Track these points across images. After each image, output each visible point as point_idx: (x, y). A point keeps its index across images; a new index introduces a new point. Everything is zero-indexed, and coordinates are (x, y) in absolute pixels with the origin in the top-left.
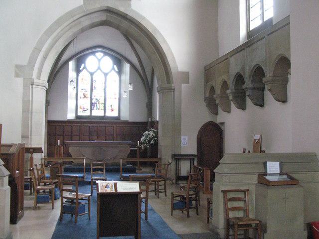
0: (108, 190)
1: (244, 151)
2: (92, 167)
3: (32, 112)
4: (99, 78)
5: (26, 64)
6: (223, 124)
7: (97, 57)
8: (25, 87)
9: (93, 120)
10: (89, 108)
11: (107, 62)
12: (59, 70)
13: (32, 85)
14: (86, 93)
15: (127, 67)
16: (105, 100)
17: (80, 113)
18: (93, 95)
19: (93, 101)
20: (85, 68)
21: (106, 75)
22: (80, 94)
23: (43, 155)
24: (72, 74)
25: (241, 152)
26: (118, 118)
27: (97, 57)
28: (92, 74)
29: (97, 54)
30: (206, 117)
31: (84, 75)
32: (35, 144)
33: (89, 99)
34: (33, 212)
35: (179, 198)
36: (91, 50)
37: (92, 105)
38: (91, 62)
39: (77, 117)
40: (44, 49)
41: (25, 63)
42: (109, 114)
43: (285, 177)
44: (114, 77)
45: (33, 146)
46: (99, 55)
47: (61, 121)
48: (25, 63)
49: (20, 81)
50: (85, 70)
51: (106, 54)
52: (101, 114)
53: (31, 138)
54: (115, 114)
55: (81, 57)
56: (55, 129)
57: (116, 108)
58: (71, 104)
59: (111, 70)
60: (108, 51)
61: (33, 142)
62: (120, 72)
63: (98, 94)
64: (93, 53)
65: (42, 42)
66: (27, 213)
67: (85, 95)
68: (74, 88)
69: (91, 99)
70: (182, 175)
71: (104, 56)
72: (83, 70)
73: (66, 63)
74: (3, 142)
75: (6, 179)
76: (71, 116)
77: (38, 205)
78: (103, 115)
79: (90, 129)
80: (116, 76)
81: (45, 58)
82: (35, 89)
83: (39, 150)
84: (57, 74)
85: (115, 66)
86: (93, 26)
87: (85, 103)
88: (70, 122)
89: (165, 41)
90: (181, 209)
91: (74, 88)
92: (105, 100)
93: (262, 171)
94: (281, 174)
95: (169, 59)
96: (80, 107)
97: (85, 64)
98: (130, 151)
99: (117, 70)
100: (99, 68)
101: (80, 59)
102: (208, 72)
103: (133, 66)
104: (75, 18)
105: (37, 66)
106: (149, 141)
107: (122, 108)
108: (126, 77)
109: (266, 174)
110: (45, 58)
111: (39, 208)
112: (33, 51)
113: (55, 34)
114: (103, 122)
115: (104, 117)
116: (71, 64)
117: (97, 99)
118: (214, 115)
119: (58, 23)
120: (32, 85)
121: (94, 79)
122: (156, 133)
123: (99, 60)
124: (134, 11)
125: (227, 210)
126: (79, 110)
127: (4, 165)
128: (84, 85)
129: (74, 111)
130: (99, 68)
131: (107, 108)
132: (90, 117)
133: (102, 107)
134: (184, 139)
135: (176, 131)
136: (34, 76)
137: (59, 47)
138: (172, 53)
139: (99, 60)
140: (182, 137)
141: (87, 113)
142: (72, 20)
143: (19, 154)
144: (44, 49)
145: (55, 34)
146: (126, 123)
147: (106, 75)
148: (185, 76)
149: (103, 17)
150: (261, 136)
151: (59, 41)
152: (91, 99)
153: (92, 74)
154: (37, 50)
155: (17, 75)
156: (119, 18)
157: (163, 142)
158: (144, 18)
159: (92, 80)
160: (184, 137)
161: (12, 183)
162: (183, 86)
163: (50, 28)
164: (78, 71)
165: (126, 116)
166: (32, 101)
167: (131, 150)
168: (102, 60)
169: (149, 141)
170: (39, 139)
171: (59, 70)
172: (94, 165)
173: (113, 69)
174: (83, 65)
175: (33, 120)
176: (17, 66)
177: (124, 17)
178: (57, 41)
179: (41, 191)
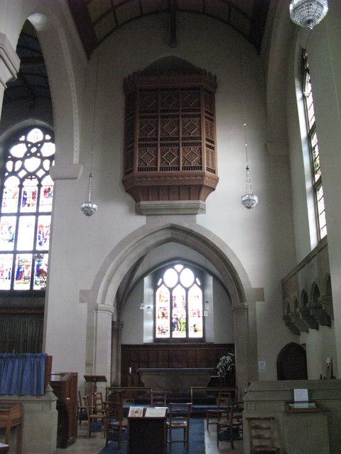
0: (137, 415)
1: (321, 378)
2: (152, 397)
3: (96, 339)
4: (179, 293)
5: (89, 288)
6: (305, 345)
7: (176, 270)
8: (90, 312)
9: (173, 344)
10: (169, 329)
11: (188, 276)
12: (133, 288)
13: (96, 310)
14: (165, 312)
15: (210, 280)
16: (187, 319)
17: (159, 336)
18: (173, 314)
19: (174, 320)
20: (163, 283)
21: (187, 290)
22: (159, 313)
23: (108, 384)
24: (148, 291)
25: (318, 378)
27: (176, 270)
28: (171, 290)
29: (176, 267)
30: (287, 338)
31: (162, 291)
33: (169, 318)
34: (87, 441)
35: (225, 429)
36: (169, 263)
37: (173, 326)
38: (170, 276)
39: (156, 340)
40: (108, 273)
41: (89, 287)
42: (192, 335)
43: (313, 404)
44: (196, 292)
45: (97, 375)
46: (179, 267)
47: (330, 287)
48: (89, 287)
50: (163, 285)
51: (185, 266)
52: (182, 335)
53: (95, 366)
54: (199, 335)
55: (157, 271)
57: (200, 327)
58: (148, 324)
59: (193, 285)
60: (188, 263)
61: (97, 370)
62: (203, 287)
63: (179, 312)
64: (172, 266)
65: (105, 266)
66: (79, 441)
67: (163, 315)
68: (11, 241)
69: (171, 319)
71: (184, 268)
72: (160, 285)
73: (141, 279)
75: (54, 404)
76: (148, 339)
77: (92, 434)
78: (185, 336)
79: (170, 353)
80: (199, 292)
81: (109, 281)
83: (103, 379)
85: (197, 279)
86: (168, 241)
87: (163, 323)
88: (146, 346)
89: (234, 255)
90: (228, 440)
91: (11, 241)
92: (187, 319)
93: (288, 398)
94: (310, 401)
95: (241, 276)
96: (159, 328)
97: (162, 278)
98: (210, 379)
99: (199, 283)
100: (179, 282)
101: (157, 273)
102: (284, 286)
103: (216, 278)
104: (138, 239)
105: (101, 291)
106: (226, 367)
107: (206, 328)
108: (210, 292)
109: (293, 402)
110: (109, 281)
111: (94, 437)
112: (97, 276)
113: (119, 256)
114: (187, 343)
115: (187, 340)
116: (147, 280)
117: (177, 319)
118: (295, 336)
119: (121, 245)
120: (96, 310)
121: (173, 295)
122: (233, 358)
123: (179, 274)
124: (198, 226)
125: (252, 437)
126: (157, 331)
127: (53, 392)
129: (152, 333)
130: (179, 282)
131: (190, 329)
132: (171, 339)
133: (183, 327)
134: (262, 364)
135: (253, 355)
136: (99, 301)
137: (133, 258)
138: (243, 269)
139: (179, 274)
140: (259, 362)
141: (167, 336)
142: (135, 241)
144: (108, 273)
145: (119, 256)
146: (211, 345)
147: (187, 290)
148: (260, 293)
149: (168, 235)
150: (331, 360)
151: (123, 263)
152: (171, 319)
153: (171, 290)
154: (101, 274)
155: (82, 301)
156: (185, 235)
157: (240, 369)
158: (210, 233)
159: (171, 297)
160: (262, 362)
161: (61, 408)
162: (258, 303)
163: (114, 250)
164: (155, 287)
165: (211, 338)
166: (96, 327)
167: (212, 378)
168: (182, 273)
169: (226, 367)
171: (133, 288)
172: (155, 395)
173: (195, 282)
174: (161, 280)
175: (98, 347)
176: (82, 292)
177: (190, 233)
178: (121, 263)
179: (98, 419)
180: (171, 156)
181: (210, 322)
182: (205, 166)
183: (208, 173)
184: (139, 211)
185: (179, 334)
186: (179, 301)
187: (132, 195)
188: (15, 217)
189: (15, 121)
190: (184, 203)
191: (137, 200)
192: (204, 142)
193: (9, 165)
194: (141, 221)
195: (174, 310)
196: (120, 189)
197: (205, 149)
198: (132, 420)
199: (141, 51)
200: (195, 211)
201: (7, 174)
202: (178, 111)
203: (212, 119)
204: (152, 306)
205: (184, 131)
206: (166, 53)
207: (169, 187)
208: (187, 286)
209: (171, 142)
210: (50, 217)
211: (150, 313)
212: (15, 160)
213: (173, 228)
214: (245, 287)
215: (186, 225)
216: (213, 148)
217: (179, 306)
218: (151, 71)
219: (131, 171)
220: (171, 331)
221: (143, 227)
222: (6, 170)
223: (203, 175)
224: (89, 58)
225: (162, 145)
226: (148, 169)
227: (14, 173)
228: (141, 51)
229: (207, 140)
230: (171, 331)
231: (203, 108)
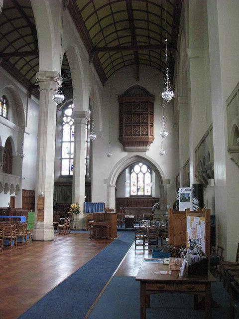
4: (141, 176)
10: (136, 191)
17: (132, 194)
19: (138, 187)
20: (134, 171)
21: (144, 174)
22: (132, 184)
24: (127, 174)
26: (150, 196)
31: (133, 175)
32: (111, 208)
37: (138, 189)
38: (137, 168)
39: (131, 196)
42: (146, 194)
44: (148, 175)
49: (105, 185)
54: (149, 194)
56: (120, 202)
57: (149, 190)
58: (127, 189)
63: (141, 184)
64: (138, 164)
65: (113, 170)
70: (228, 261)
74: (132, 2)
76: (127, 195)
78: (143, 194)
81: (114, 176)
82: (111, 188)
84: (121, 178)
87: (134, 189)
95: (162, 174)
100: (141, 171)
110: (114, 176)
115: (144, 196)
123: (141, 167)
128: (134, 180)
130: (141, 171)
132: (137, 196)
133: (142, 190)
139: (141, 167)
141: (135, 194)
143: (194, 203)
146: (154, 198)
147: (144, 174)
153: (137, 174)
164: (130, 173)
165: (154, 195)
170: (112, 206)
173: (148, 171)
176: (105, 180)
180: (136, 130)
181: (154, 188)
182: (149, 134)
183: (150, 137)
184: (125, 150)
185: (141, 193)
186: (141, 179)
187: (122, 144)
188: (69, 143)
189: (68, 99)
190: (141, 147)
191: (124, 146)
192: (149, 124)
193: (65, 119)
194: (125, 154)
195: (138, 183)
196: (118, 142)
197: (149, 127)
198: (127, 218)
199: (124, 82)
200: (145, 151)
201: (64, 123)
202: (139, 112)
203: (152, 114)
204: (129, 182)
205: (142, 132)
206: (133, 83)
207: (136, 142)
208: (144, 173)
209: (137, 124)
210: (13, 63)
211: (129, 185)
212: (67, 116)
213: (137, 156)
214: (163, 179)
215: (142, 156)
216: (153, 126)
217: (141, 183)
218: (128, 92)
219: (122, 136)
220: (137, 192)
221: (127, 156)
222: (63, 121)
223: (148, 138)
224: (103, 85)
225: (133, 126)
226: (128, 135)
227: (67, 123)
228: (124, 82)
229: (150, 123)
230: (137, 192)
231: (149, 110)
